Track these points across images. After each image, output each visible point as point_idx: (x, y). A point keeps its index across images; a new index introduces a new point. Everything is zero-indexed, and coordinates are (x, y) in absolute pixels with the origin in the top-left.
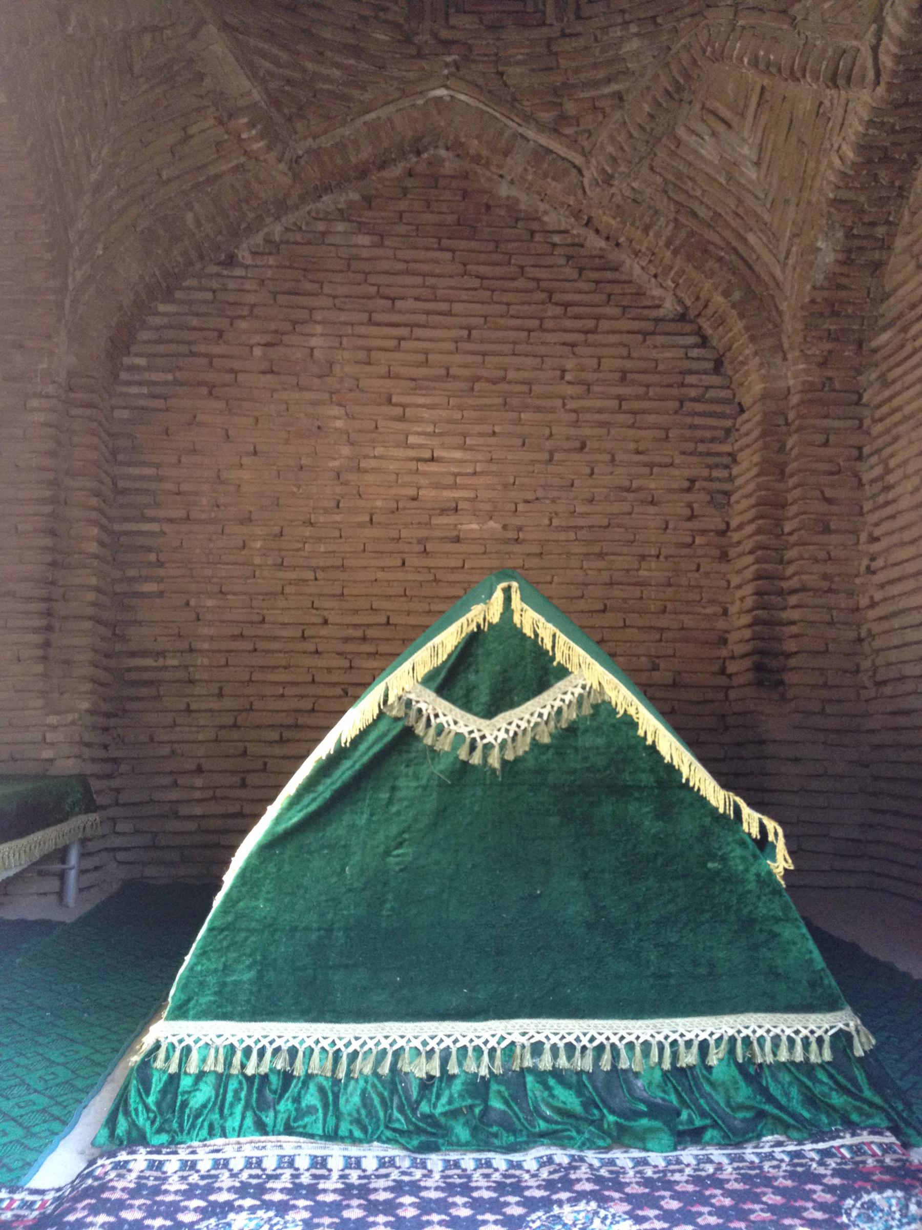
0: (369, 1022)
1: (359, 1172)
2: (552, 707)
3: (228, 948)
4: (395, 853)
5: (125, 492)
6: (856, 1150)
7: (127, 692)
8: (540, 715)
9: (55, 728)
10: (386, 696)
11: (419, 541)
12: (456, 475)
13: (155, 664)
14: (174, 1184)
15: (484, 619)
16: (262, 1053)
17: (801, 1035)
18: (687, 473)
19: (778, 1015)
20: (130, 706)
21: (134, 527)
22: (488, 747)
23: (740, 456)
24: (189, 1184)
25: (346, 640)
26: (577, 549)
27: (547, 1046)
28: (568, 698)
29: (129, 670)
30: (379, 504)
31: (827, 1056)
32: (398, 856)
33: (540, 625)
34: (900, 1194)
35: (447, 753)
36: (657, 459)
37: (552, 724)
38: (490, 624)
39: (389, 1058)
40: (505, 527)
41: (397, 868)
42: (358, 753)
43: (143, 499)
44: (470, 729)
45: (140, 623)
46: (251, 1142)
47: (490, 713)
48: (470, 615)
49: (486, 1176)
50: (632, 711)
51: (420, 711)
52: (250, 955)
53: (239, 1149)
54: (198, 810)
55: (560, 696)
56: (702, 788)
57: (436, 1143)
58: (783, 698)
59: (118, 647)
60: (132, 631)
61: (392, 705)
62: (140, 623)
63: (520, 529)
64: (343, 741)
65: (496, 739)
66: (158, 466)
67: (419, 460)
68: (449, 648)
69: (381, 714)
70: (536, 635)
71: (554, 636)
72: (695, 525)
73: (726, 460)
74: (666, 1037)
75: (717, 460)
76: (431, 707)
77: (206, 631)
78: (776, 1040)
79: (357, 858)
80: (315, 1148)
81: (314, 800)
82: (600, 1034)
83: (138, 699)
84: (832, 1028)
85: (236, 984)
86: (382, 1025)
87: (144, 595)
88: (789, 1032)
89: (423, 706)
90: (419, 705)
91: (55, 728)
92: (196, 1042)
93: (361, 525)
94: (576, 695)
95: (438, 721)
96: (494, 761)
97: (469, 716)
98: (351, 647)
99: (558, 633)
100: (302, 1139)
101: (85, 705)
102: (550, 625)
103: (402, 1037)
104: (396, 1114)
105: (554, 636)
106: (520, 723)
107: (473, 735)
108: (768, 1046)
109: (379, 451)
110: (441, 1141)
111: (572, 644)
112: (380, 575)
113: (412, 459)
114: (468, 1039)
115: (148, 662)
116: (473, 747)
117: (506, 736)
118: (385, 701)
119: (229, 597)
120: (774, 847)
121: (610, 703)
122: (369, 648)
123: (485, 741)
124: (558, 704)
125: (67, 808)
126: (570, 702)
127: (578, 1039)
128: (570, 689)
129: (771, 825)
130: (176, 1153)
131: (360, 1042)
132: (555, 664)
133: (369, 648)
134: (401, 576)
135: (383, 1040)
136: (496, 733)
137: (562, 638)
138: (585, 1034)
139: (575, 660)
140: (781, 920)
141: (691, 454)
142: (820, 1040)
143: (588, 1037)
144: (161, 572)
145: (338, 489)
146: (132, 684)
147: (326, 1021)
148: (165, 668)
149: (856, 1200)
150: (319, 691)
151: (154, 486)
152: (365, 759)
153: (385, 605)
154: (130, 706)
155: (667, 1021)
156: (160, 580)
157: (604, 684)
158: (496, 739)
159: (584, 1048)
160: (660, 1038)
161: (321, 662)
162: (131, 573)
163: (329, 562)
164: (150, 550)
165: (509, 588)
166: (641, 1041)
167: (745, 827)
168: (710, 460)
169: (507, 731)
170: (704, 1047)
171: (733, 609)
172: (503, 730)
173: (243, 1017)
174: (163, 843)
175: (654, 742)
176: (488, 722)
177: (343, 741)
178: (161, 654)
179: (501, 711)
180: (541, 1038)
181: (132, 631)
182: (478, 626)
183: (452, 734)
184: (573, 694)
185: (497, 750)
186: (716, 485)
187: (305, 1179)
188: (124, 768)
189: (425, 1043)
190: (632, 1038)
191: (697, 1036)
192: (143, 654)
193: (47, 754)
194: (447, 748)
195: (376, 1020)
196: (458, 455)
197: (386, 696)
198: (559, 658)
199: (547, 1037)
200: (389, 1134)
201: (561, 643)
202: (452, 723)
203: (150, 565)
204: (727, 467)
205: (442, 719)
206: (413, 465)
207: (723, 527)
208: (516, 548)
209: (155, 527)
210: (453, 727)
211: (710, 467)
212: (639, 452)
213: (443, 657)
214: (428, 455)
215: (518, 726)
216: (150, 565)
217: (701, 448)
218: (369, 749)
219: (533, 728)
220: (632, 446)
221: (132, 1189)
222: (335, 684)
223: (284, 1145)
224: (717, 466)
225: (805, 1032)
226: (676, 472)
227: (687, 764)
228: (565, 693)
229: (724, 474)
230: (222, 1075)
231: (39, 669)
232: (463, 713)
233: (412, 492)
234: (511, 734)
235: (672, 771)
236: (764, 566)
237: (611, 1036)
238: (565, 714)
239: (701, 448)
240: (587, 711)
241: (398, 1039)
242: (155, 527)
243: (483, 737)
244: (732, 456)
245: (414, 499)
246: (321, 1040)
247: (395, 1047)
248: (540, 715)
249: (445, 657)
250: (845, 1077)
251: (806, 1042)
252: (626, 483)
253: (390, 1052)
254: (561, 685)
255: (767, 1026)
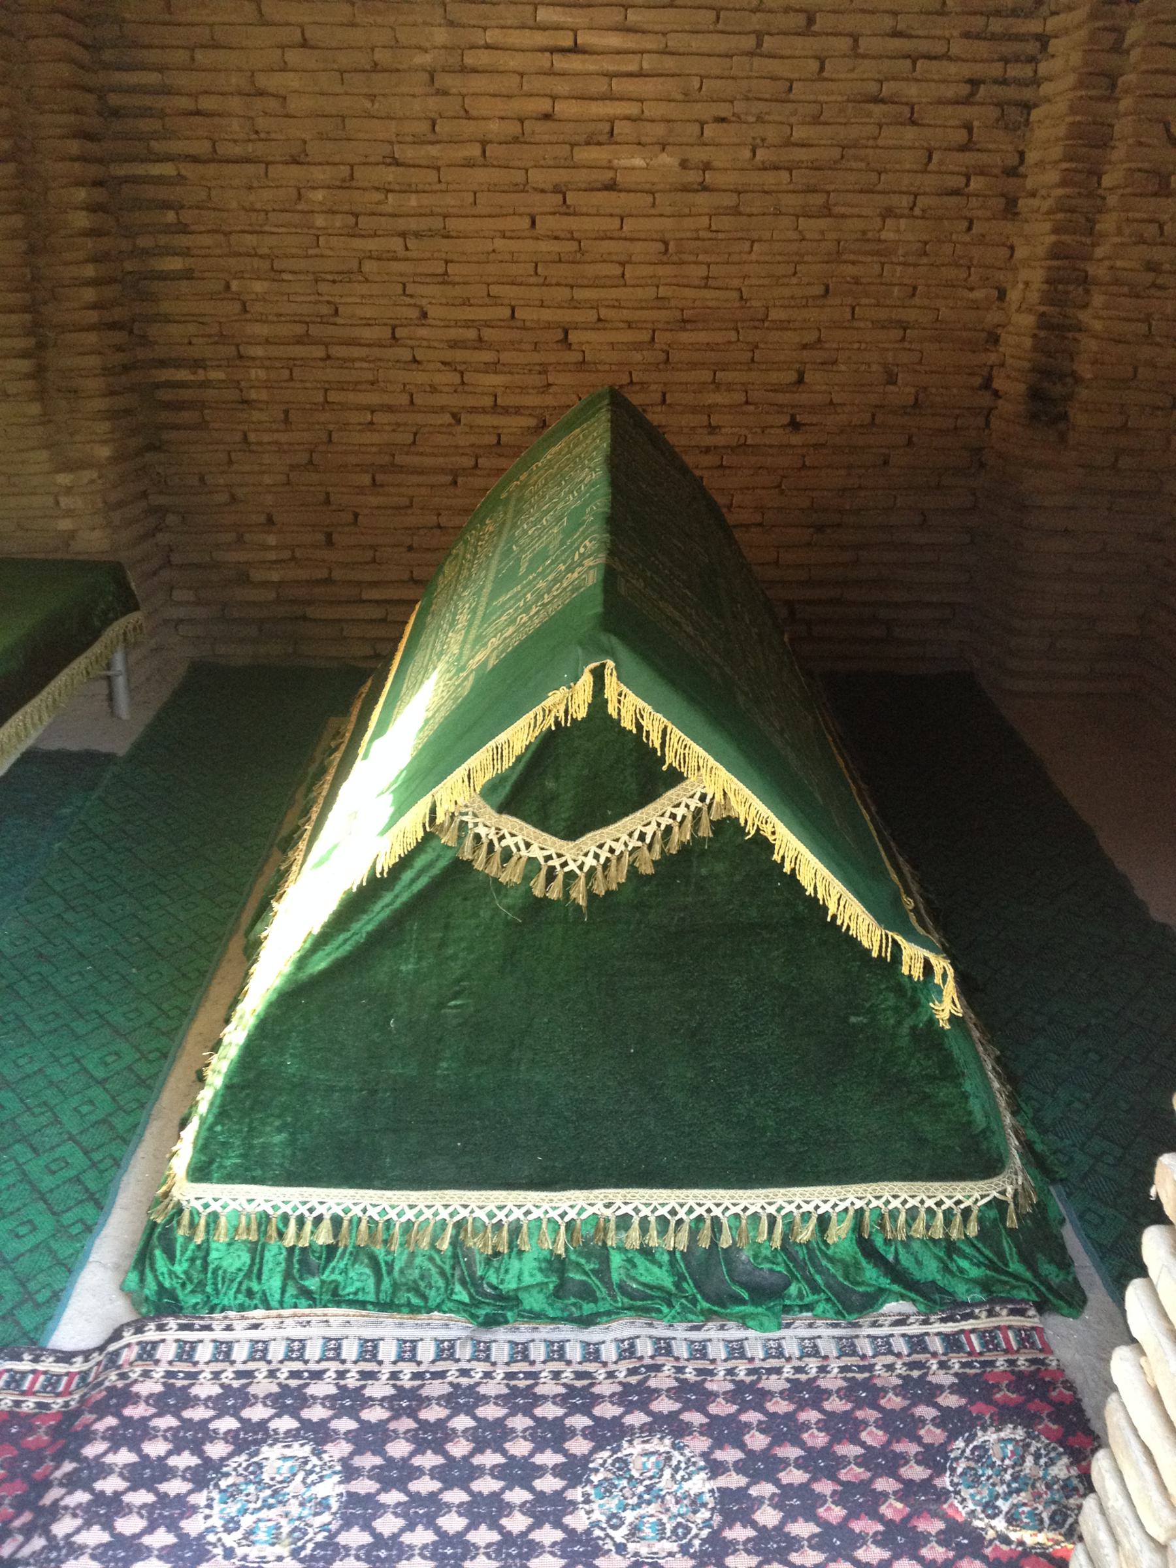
0: (426, 1189)
1: (413, 1368)
2: (659, 825)
3: (252, 1109)
4: (453, 1003)
5: (116, 113)
6: (989, 1338)
7: (164, 416)
8: (642, 837)
9: (69, 491)
10: (433, 811)
11: (557, 190)
12: (611, 76)
13: (192, 378)
14: (206, 1389)
15: (566, 712)
16: (301, 1221)
17: (944, 1207)
18: (967, 70)
19: (918, 1184)
20: (166, 436)
21: (140, 170)
22: (571, 877)
23: (1055, 45)
24: (222, 1386)
25: (454, 345)
26: (791, 202)
27: (636, 1221)
28: (680, 812)
29: (157, 386)
30: (494, 126)
31: (973, 1229)
32: (456, 1007)
33: (646, 715)
34: (1020, 1434)
35: (517, 886)
36: (924, 46)
37: (657, 847)
38: (574, 720)
39: (450, 1231)
40: (684, 164)
41: (455, 1022)
42: (398, 888)
43: (146, 125)
44: (547, 853)
45: (167, 319)
46: (294, 1316)
47: (571, 833)
48: (547, 703)
49: (556, 1375)
50: (767, 831)
51: (477, 837)
52: (279, 1116)
53: (280, 1326)
54: (275, 576)
55: (670, 810)
56: (853, 926)
57: (504, 1316)
58: (1063, 438)
59: (142, 354)
60: (154, 330)
61: (442, 825)
62: (167, 319)
63: (706, 167)
64: (378, 870)
65: (581, 867)
66: (161, 69)
67: (553, 50)
68: (519, 747)
69: (428, 837)
70: (639, 727)
71: (664, 731)
72: (969, 158)
73: (1031, 48)
74: (779, 1210)
75: (1017, 47)
76: (493, 830)
77: (262, 330)
78: (913, 1213)
79: (401, 1010)
80: (367, 1325)
81: (345, 941)
82: (700, 1205)
83: (176, 427)
84: (983, 1197)
85: (264, 1147)
86: (440, 1193)
87: (164, 276)
88: (930, 1203)
89: (482, 831)
90: (477, 830)
91: (69, 491)
92: (224, 1207)
93: (469, 164)
94: (692, 808)
95: (504, 843)
96: (579, 894)
97: (546, 836)
98: (459, 355)
99: (670, 726)
100: (352, 1311)
101: (104, 452)
102: (659, 716)
103: (466, 1206)
104: (458, 1288)
105: (664, 731)
106: (614, 845)
107: (550, 863)
108: (902, 1218)
109: (492, 36)
110: (509, 1314)
111: (689, 741)
112: (499, 243)
113: (542, 50)
114: (542, 1210)
115: (183, 375)
116: (551, 875)
117: (594, 863)
118: (433, 819)
119: (285, 276)
120: (940, 992)
121: (737, 819)
122: (487, 356)
123: (567, 869)
124: (666, 821)
125: (97, 623)
126: (684, 817)
127: (673, 1212)
128: (685, 800)
129: (940, 964)
130: (208, 1328)
131: (415, 1210)
132: (664, 768)
133: (487, 356)
134: (529, 245)
135: (441, 1210)
136: (581, 858)
137: (676, 734)
138: (682, 1205)
139: (693, 764)
140: (935, 1078)
141: (978, 37)
142: (966, 1212)
143: (686, 1208)
144: (183, 241)
145: (433, 104)
146: (168, 406)
147: (374, 1188)
148: (204, 384)
149: (968, 1442)
150: (420, 418)
151: (160, 102)
152: (405, 897)
153: (509, 292)
154: (166, 436)
155: (782, 1191)
156: (186, 253)
157: (730, 795)
158: (581, 867)
159: (680, 1222)
160: (771, 1210)
161: (421, 378)
162: (143, 242)
163: (423, 224)
164: (166, 205)
165: (603, 666)
166: (748, 1213)
167: (905, 970)
168: (1008, 48)
169: (596, 856)
170: (824, 1222)
171: (1014, 295)
172: (591, 855)
173: (277, 1181)
174: (236, 614)
175: (793, 870)
176: (571, 844)
177: (378, 870)
178: (198, 364)
179: (590, 831)
180: (628, 1210)
181: (154, 330)
182: (557, 723)
183: (523, 860)
184: (687, 806)
185: (582, 881)
186: (1011, 93)
187: (351, 1382)
188: (171, 519)
189: (491, 1215)
190: (738, 1210)
191: (817, 1207)
192: (178, 363)
193: (65, 524)
194: (516, 879)
195: (433, 1188)
196: (614, 40)
197: (433, 811)
198: (670, 758)
199: (637, 1210)
200: (450, 1305)
201: (674, 740)
202: (522, 846)
203: (168, 229)
204: (1032, 59)
205: (509, 841)
206: (544, 60)
207: (1013, 160)
208: (702, 199)
209: (168, 169)
210: (524, 853)
211: (1005, 60)
212: (896, 34)
213: (508, 763)
214: (568, 42)
215: (612, 851)
216: (168, 229)
217: (996, 25)
218: (413, 881)
219: (631, 853)
220: (887, 22)
221: (160, 1394)
222: (442, 409)
223: (331, 1319)
224: (1017, 59)
225: (948, 1203)
226: (953, 69)
227: (835, 898)
228: (678, 805)
229: (1027, 71)
230: (256, 1243)
231: (35, 409)
232: (538, 832)
233: (544, 105)
234: (602, 860)
235: (816, 907)
236: (1066, 238)
237: (713, 1208)
238: (676, 836)
239: (996, 25)
240: (705, 831)
241: (460, 1209)
242: (168, 169)
243: (564, 864)
244: (1043, 40)
245: (547, 117)
246: (369, 1208)
247: (457, 1218)
248: (642, 837)
249: (513, 760)
250: (991, 1250)
251: (948, 1215)
252: (872, 88)
253: (450, 1223)
254: (672, 794)
255: (904, 1196)
